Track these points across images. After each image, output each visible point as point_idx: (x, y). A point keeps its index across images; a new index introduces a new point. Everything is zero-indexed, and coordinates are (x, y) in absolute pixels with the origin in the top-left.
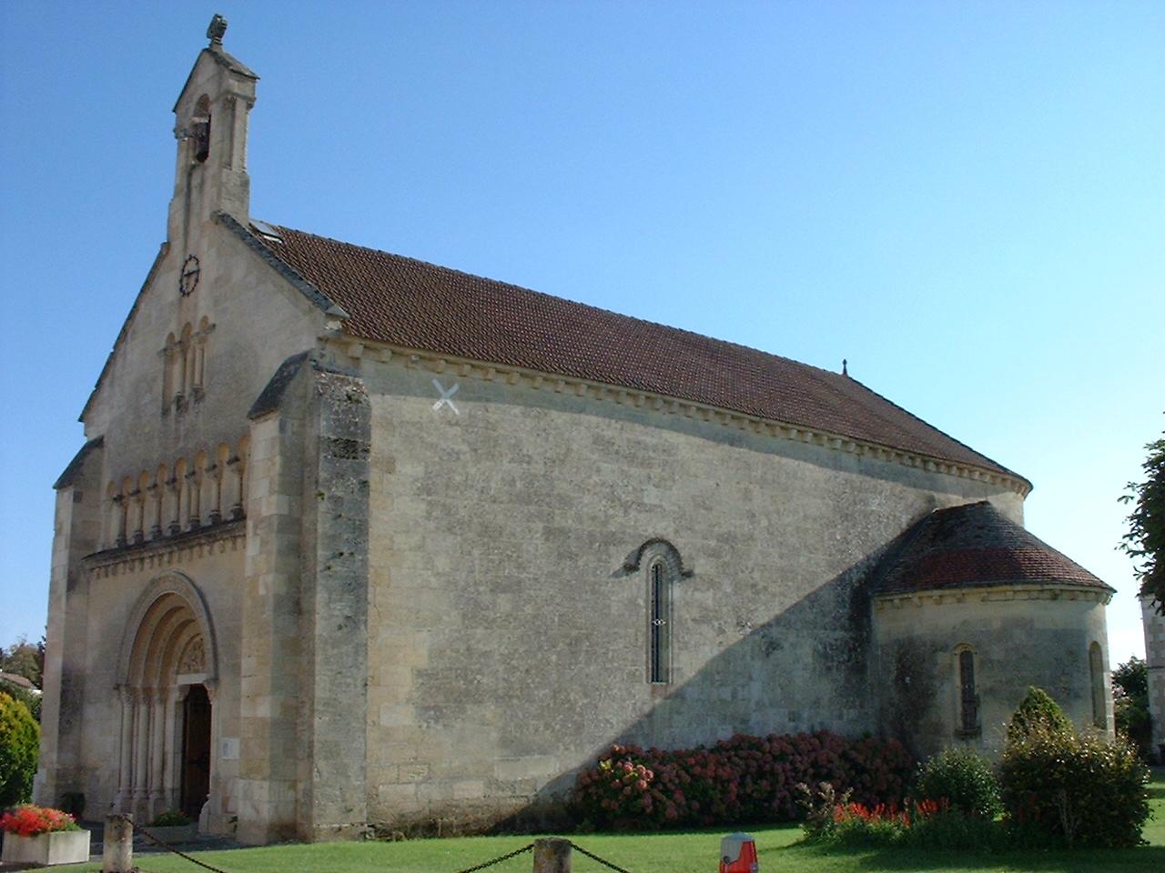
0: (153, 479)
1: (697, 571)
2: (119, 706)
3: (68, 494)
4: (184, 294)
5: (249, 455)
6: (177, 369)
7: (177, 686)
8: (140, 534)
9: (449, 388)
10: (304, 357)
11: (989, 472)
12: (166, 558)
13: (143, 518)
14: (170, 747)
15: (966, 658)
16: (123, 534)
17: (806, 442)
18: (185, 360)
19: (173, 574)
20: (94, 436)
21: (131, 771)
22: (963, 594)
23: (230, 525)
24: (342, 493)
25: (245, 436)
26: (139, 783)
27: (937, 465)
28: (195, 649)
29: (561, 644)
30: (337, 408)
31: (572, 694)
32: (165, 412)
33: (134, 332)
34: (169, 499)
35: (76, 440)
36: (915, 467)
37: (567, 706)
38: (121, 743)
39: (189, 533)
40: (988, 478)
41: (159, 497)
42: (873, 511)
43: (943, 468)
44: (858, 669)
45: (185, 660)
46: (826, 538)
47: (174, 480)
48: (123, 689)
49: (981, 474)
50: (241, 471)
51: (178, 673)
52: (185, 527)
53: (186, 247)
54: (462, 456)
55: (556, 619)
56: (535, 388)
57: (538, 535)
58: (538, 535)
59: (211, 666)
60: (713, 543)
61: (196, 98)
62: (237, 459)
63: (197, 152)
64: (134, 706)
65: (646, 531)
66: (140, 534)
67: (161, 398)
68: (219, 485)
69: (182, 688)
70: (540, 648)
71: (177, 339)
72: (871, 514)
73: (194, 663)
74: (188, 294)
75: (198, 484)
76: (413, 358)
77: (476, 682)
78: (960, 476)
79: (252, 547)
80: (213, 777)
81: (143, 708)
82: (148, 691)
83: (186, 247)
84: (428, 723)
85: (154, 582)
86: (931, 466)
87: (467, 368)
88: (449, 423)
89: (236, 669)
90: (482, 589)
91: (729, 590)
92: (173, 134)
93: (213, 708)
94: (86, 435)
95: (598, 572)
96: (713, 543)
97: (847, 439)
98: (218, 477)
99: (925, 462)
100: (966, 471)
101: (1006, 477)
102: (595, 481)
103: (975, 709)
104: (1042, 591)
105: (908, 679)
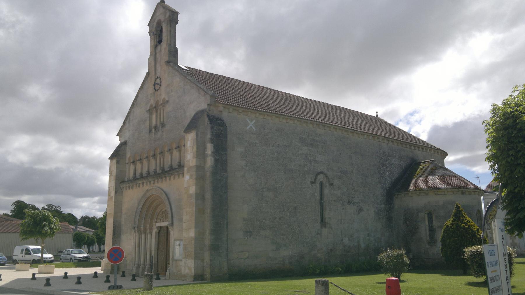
0: (146, 155)
1: (334, 184)
2: (135, 234)
3: (115, 161)
4: (156, 90)
5: (184, 146)
6: (154, 116)
7: (156, 227)
8: (141, 174)
9: (252, 122)
10: (202, 111)
11: (433, 149)
12: (152, 182)
13: (143, 168)
14: (153, 249)
15: (430, 215)
16: (135, 174)
17: (370, 139)
18: (157, 113)
19: (155, 187)
20: (123, 141)
21: (139, 258)
22: (428, 192)
23: (177, 170)
24: (218, 158)
25: (183, 138)
26: (142, 262)
27: (414, 147)
28: (163, 214)
29: (291, 209)
30: (216, 128)
31: (295, 227)
32: (150, 131)
33: (137, 104)
34: (153, 161)
35: (116, 142)
36: (406, 148)
37: (293, 231)
38: (136, 247)
39: (161, 173)
40: (432, 152)
41: (149, 161)
42: (393, 163)
43: (416, 148)
44: (390, 219)
45: (159, 217)
46: (377, 173)
47: (154, 155)
48: (136, 229)
49: (430, 150)
50: (180, 151)
51: (156, 222)
52: (159, 171)
53: (156, 73)
54: (257, 145)
55: (289, 200)
56: (280, 121)
57: (282, 171)
58: (282, 171)
59: (170, 219)
60: (339, 174)
61: (156, 21)
62: (179, 147)
63: (157, 41)
64: (140, 235)
65: (317, 170)
66: (141, 174)
67: (148, 127)
68: (172, 156)
69: (158, 227)
70: (284, 210)
71: (154, 105)
72: (392, 164)
73: (162, 219)
74: (157, 90)
75: (164, 156)
76: (240, 111)
77: (263, 222)
78: (422, 151)
79: (187, 177)
80: (171, 259)
81: (143, 236)
82: (145, 229)
83: (156, 73)
84: (248, 237)
85: (147, 191)
86: (412, 148)
87: (258, 114)
88: (253, 134)
89: (181, 220)
90: (264, 190)
91: (345, 190)
92: (148, 34)
93: (171, 234)
94: (119, 141)
95: (302, 184)
96: (339, 174)
97: (383, 138)
98: (171, 154)
99: (410, 146)
100: (425, 149)
101: (439, 151)
102: (300, 153)
103: (434, 233)
104: (458, 191)
105: (408, 222)
